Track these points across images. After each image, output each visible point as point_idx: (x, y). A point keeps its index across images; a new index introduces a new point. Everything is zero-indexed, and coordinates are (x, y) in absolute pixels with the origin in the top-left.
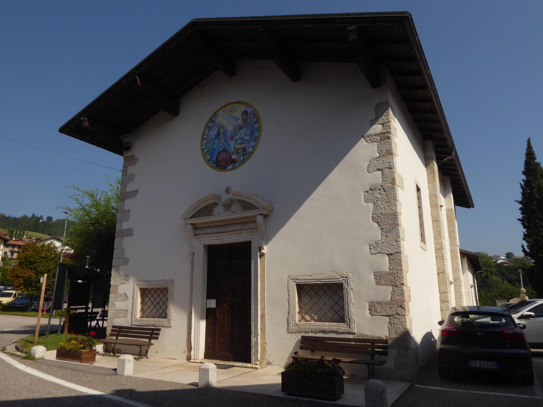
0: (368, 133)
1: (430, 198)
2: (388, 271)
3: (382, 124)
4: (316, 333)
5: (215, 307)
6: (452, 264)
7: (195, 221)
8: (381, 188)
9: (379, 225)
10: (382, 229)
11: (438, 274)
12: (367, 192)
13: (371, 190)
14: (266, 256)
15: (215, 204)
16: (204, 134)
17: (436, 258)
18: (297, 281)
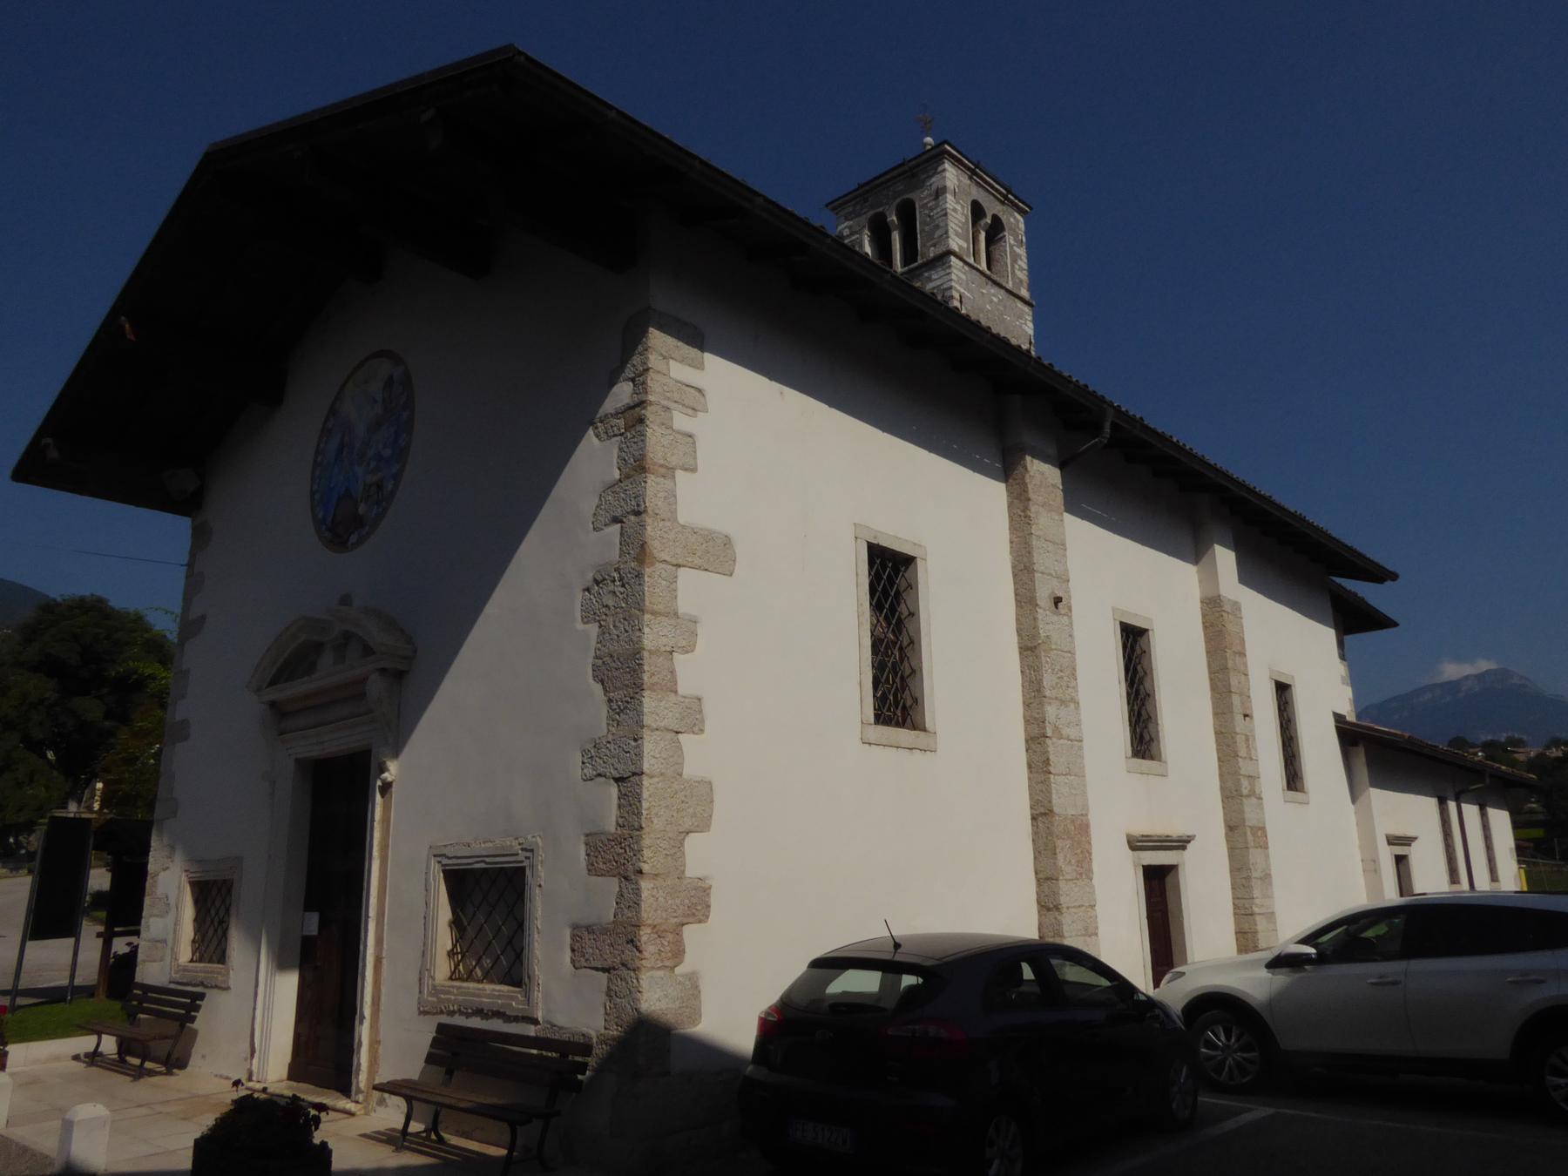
0: (601, 412)
1: (1015, 576)
2: (613, 830)
3: (633, 380)
4: (468, 1016)
5: (315, 933)
6: (1221, 776)
7: (276, 694)
8: (616, 575)
9: (606, 691)
10: (610, 701)
11: (1034, 818)
12: (588, 590)
13: (597, 582)
14: (394, 789)
15: (318, 647)
16: (317, 453)
17: (1029, 766)
18: (445, 861)
